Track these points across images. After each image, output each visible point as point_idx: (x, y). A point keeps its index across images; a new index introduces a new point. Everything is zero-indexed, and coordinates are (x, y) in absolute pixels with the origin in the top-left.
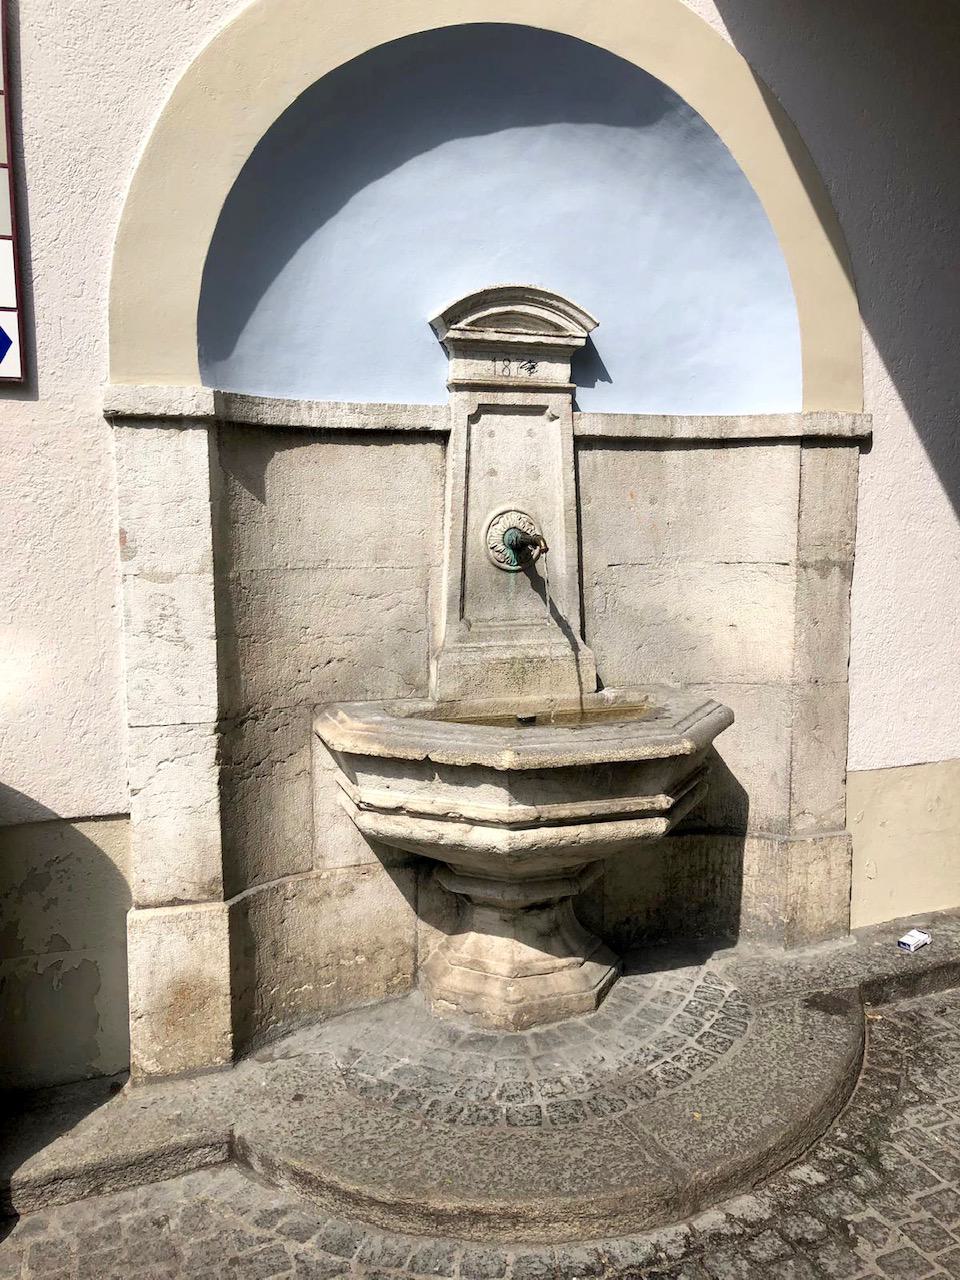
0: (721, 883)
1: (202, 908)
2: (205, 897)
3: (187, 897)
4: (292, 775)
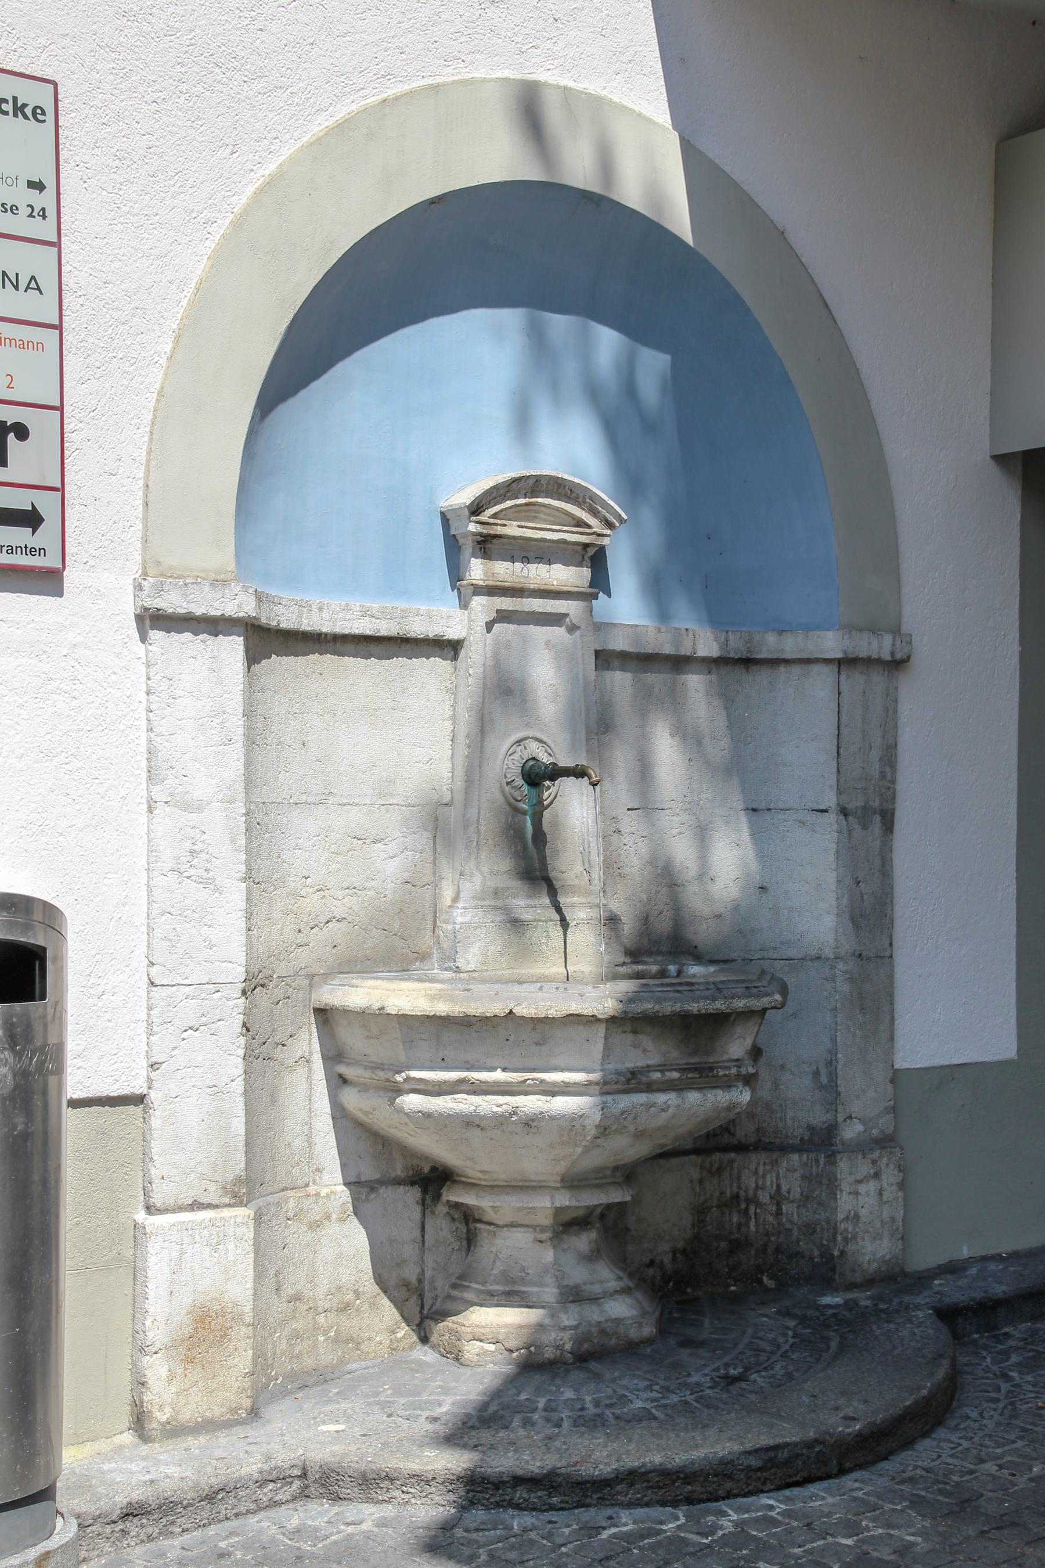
0: (756, 1214)
1: (226, 1213)
2: (227, 1200)
3: (209, 1200)
4: (291, 1062)
